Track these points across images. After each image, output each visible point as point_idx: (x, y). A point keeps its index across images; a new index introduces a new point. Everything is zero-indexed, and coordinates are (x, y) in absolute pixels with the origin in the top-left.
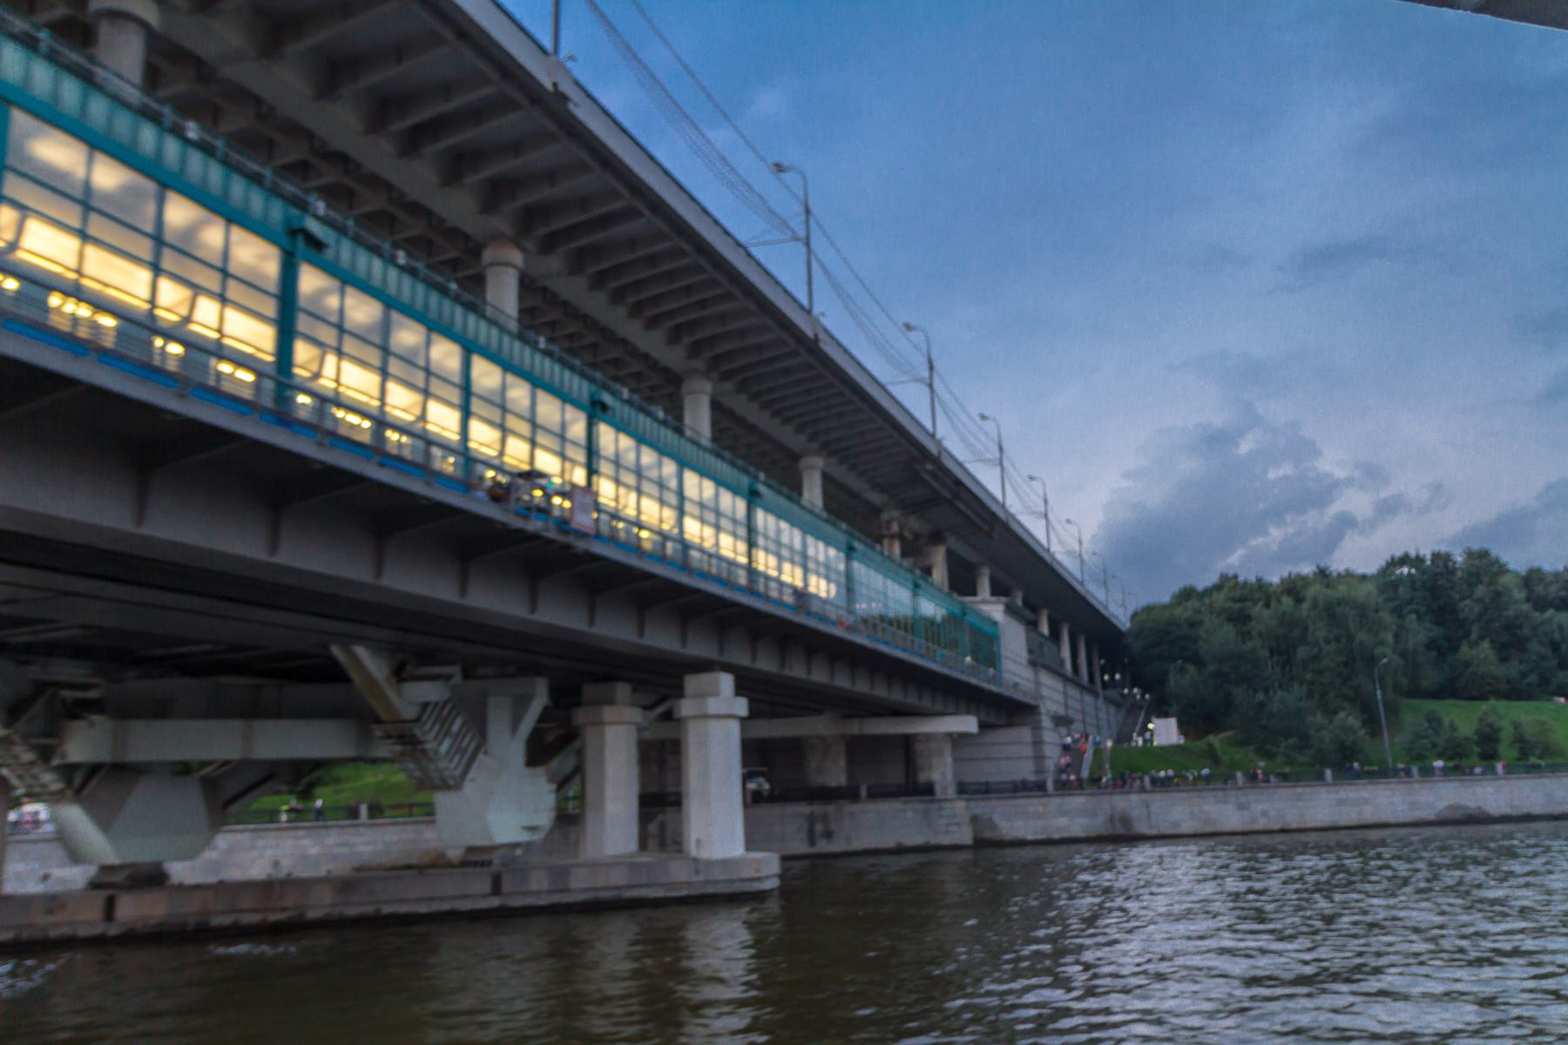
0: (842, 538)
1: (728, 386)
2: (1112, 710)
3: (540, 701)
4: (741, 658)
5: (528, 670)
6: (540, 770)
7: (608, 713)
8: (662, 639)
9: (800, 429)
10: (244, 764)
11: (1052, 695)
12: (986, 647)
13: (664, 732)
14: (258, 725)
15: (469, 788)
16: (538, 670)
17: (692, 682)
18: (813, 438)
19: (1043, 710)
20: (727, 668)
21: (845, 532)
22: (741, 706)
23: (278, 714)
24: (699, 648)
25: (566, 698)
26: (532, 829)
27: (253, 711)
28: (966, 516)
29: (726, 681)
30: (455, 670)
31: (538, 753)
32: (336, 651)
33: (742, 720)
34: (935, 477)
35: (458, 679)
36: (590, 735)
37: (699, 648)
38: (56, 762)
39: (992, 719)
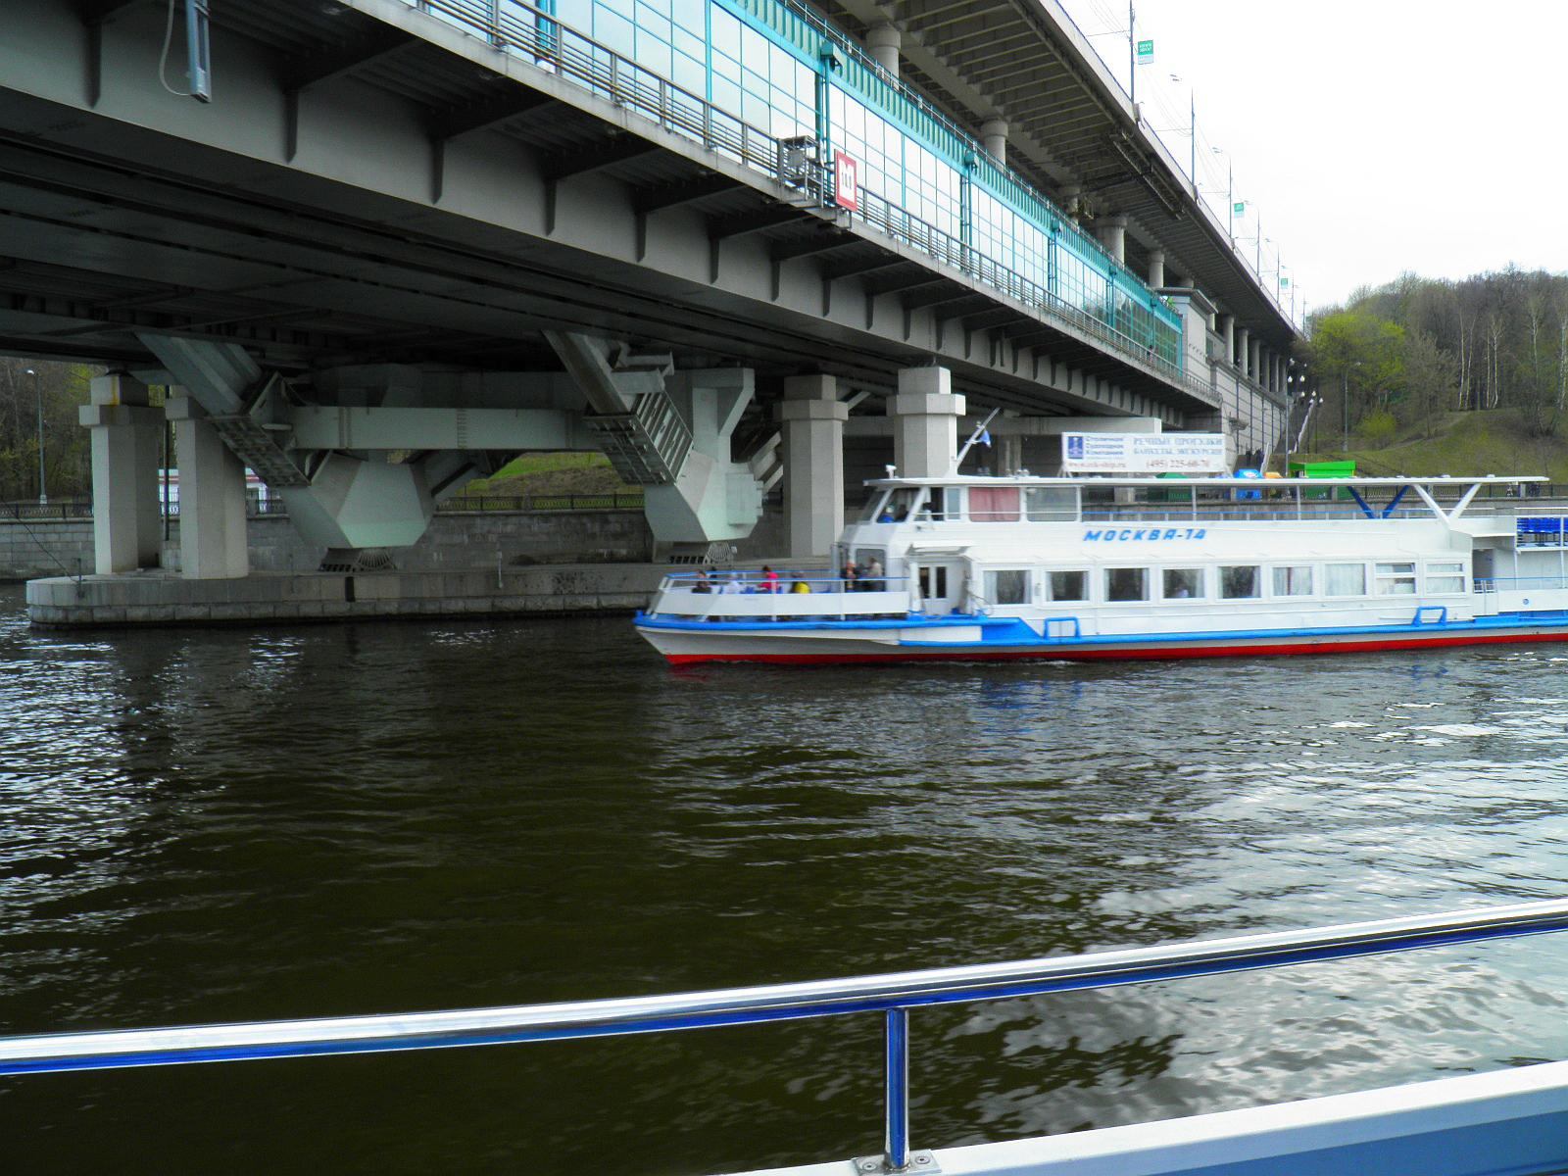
0: (1049, 217)
1: (917, 37)
2: (1276, 411)
3: (747, 394)
4: (954, 349)
5: (729, 361)
6: (744, 466)
7: (815, 408)
8: (887, 328)
9: (988, 90)
10: (463, 453)
11: (1229, 394)
12: (1170, 346)
13: (871, 427)
14: (470, 412)
15: (313, 489)
16: (745, 361)
17: (907, 377)
18: (1000, 100)
19: (1223, 414)
20: (946, 362)
21: (1049, 211)
22: (960, 404)
23: (483, 404)
24: (921, 339)
25: (770, 392)
26: (738, 526)
27: (459, 401)
28: (1154, 194)
29: (945, 376)
30: (669, 359)
31: (743, 447)
32: (552, 339)
33: (959, 418)
34: (1128, 148)
35: (670, 369)
36: (795, 430)
37: (921, 339)
38: (292, 445)
39: (1171, 422)
